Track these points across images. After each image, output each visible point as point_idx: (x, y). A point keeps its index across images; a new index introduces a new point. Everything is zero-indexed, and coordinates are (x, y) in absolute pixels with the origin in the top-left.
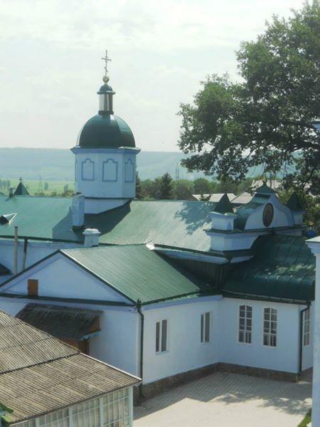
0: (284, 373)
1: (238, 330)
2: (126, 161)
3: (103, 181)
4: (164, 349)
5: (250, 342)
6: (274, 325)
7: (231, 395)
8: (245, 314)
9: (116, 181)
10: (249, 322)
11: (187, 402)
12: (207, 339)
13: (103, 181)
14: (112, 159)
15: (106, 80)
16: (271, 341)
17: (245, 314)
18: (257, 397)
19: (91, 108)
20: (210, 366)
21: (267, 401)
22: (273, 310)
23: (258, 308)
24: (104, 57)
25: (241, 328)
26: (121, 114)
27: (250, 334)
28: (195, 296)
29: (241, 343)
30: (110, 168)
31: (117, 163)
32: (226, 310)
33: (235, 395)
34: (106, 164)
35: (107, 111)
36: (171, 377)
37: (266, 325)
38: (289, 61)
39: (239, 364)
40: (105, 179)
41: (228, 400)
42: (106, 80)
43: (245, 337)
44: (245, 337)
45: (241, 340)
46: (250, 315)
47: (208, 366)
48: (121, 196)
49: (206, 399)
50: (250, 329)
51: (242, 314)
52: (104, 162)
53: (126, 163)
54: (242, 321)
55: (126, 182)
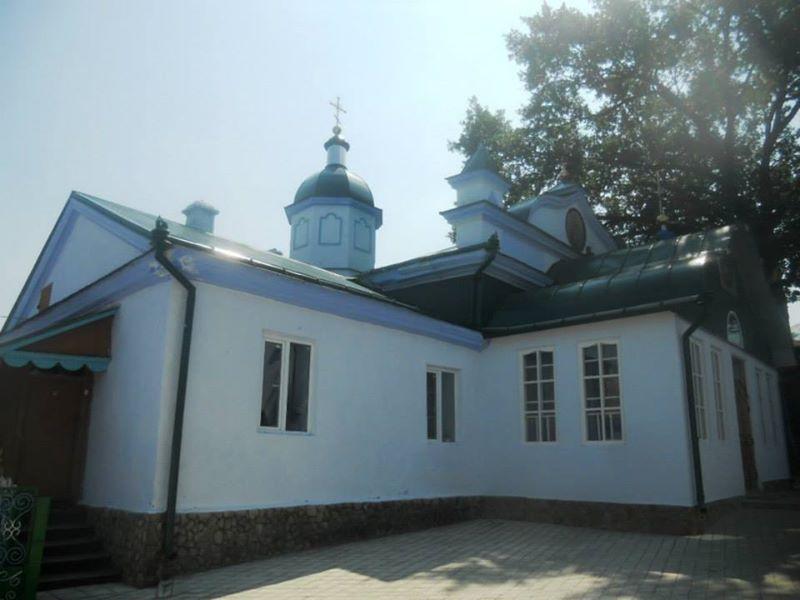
0: (653, 508)
1: (522, 413)
2: (358, 218)
3: (320, 244)
4: (297, 420)
5: (553, 438)
6: (613, 388)
7: (484, 562)
8: (539, 367)
9: (339, 244)
10: (549, 391)
11: (337, 573)
12: (448, 436)
13: (320, 244)
14: (332, 214)
15: (337, 131)
16: (605, 425)
17: (539, 367)
18: (571, 569)
19: (316, 164)
20: (457, 500)
21: (603, 581)
22: (604, 347)
23: (567, 348)
24: (335, 102)
25: (531, 407)
26: (356, 171)
27: (553, 421)
28: (311, 200)
29: (532, 444)
30: (331, 225)
31: (340, 218)
32: (492, 372)
33: (493, 560)
34: (324, 220)
35: (334, 165)
36: (318, 508)
37: (592, 388)
38: (620, 154)
39: (529, 497)
40: (322, 241)
41: (462, 577)
42: (337, 131)
43: (541, 428)
44: (541, 428)
45: (531, 436)
46: (548, 373)
47: (450, 500)
48: (346, 266)
49: (390, 572)
50: (551, 406)
51: (530, 374)
52: (322, 218)
53: (356, 222)
54: (531, 392)
55: (356, 248)
